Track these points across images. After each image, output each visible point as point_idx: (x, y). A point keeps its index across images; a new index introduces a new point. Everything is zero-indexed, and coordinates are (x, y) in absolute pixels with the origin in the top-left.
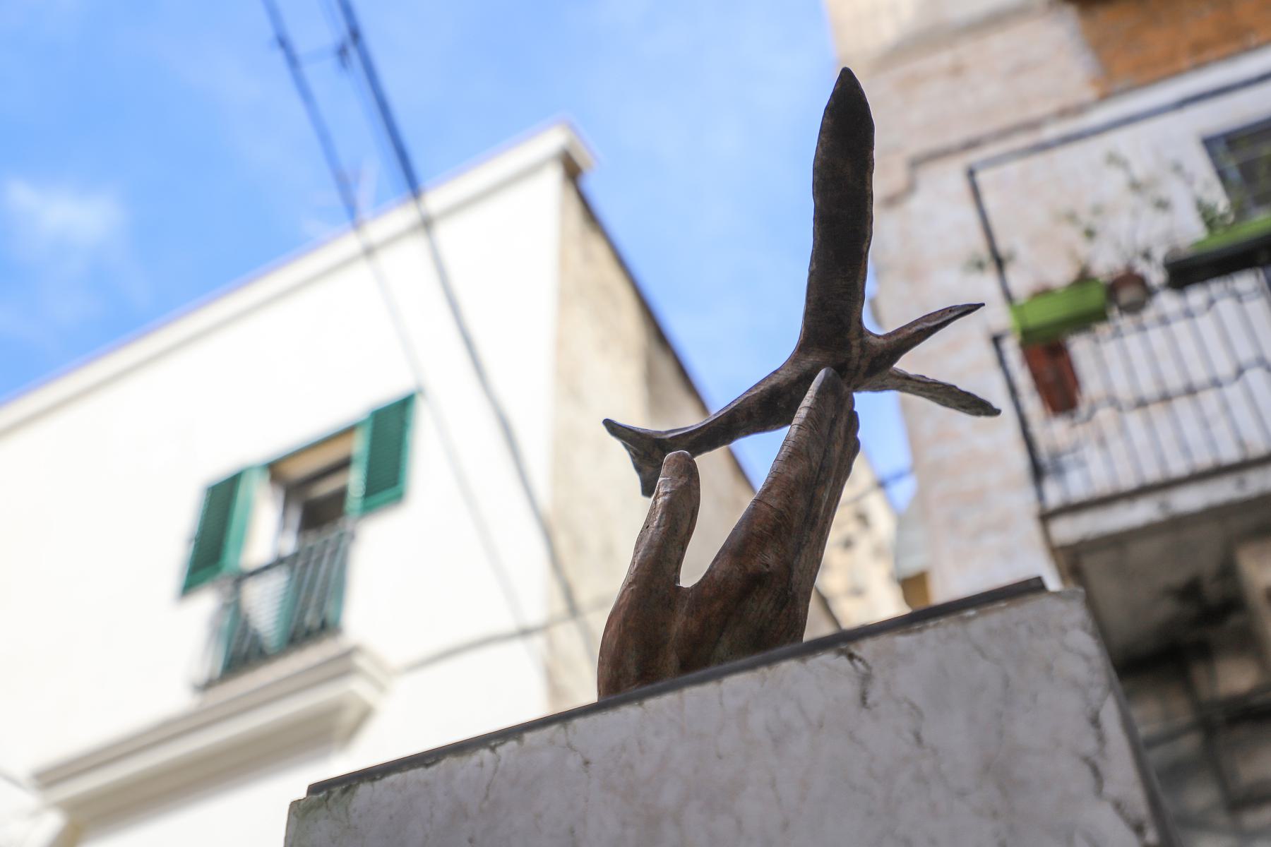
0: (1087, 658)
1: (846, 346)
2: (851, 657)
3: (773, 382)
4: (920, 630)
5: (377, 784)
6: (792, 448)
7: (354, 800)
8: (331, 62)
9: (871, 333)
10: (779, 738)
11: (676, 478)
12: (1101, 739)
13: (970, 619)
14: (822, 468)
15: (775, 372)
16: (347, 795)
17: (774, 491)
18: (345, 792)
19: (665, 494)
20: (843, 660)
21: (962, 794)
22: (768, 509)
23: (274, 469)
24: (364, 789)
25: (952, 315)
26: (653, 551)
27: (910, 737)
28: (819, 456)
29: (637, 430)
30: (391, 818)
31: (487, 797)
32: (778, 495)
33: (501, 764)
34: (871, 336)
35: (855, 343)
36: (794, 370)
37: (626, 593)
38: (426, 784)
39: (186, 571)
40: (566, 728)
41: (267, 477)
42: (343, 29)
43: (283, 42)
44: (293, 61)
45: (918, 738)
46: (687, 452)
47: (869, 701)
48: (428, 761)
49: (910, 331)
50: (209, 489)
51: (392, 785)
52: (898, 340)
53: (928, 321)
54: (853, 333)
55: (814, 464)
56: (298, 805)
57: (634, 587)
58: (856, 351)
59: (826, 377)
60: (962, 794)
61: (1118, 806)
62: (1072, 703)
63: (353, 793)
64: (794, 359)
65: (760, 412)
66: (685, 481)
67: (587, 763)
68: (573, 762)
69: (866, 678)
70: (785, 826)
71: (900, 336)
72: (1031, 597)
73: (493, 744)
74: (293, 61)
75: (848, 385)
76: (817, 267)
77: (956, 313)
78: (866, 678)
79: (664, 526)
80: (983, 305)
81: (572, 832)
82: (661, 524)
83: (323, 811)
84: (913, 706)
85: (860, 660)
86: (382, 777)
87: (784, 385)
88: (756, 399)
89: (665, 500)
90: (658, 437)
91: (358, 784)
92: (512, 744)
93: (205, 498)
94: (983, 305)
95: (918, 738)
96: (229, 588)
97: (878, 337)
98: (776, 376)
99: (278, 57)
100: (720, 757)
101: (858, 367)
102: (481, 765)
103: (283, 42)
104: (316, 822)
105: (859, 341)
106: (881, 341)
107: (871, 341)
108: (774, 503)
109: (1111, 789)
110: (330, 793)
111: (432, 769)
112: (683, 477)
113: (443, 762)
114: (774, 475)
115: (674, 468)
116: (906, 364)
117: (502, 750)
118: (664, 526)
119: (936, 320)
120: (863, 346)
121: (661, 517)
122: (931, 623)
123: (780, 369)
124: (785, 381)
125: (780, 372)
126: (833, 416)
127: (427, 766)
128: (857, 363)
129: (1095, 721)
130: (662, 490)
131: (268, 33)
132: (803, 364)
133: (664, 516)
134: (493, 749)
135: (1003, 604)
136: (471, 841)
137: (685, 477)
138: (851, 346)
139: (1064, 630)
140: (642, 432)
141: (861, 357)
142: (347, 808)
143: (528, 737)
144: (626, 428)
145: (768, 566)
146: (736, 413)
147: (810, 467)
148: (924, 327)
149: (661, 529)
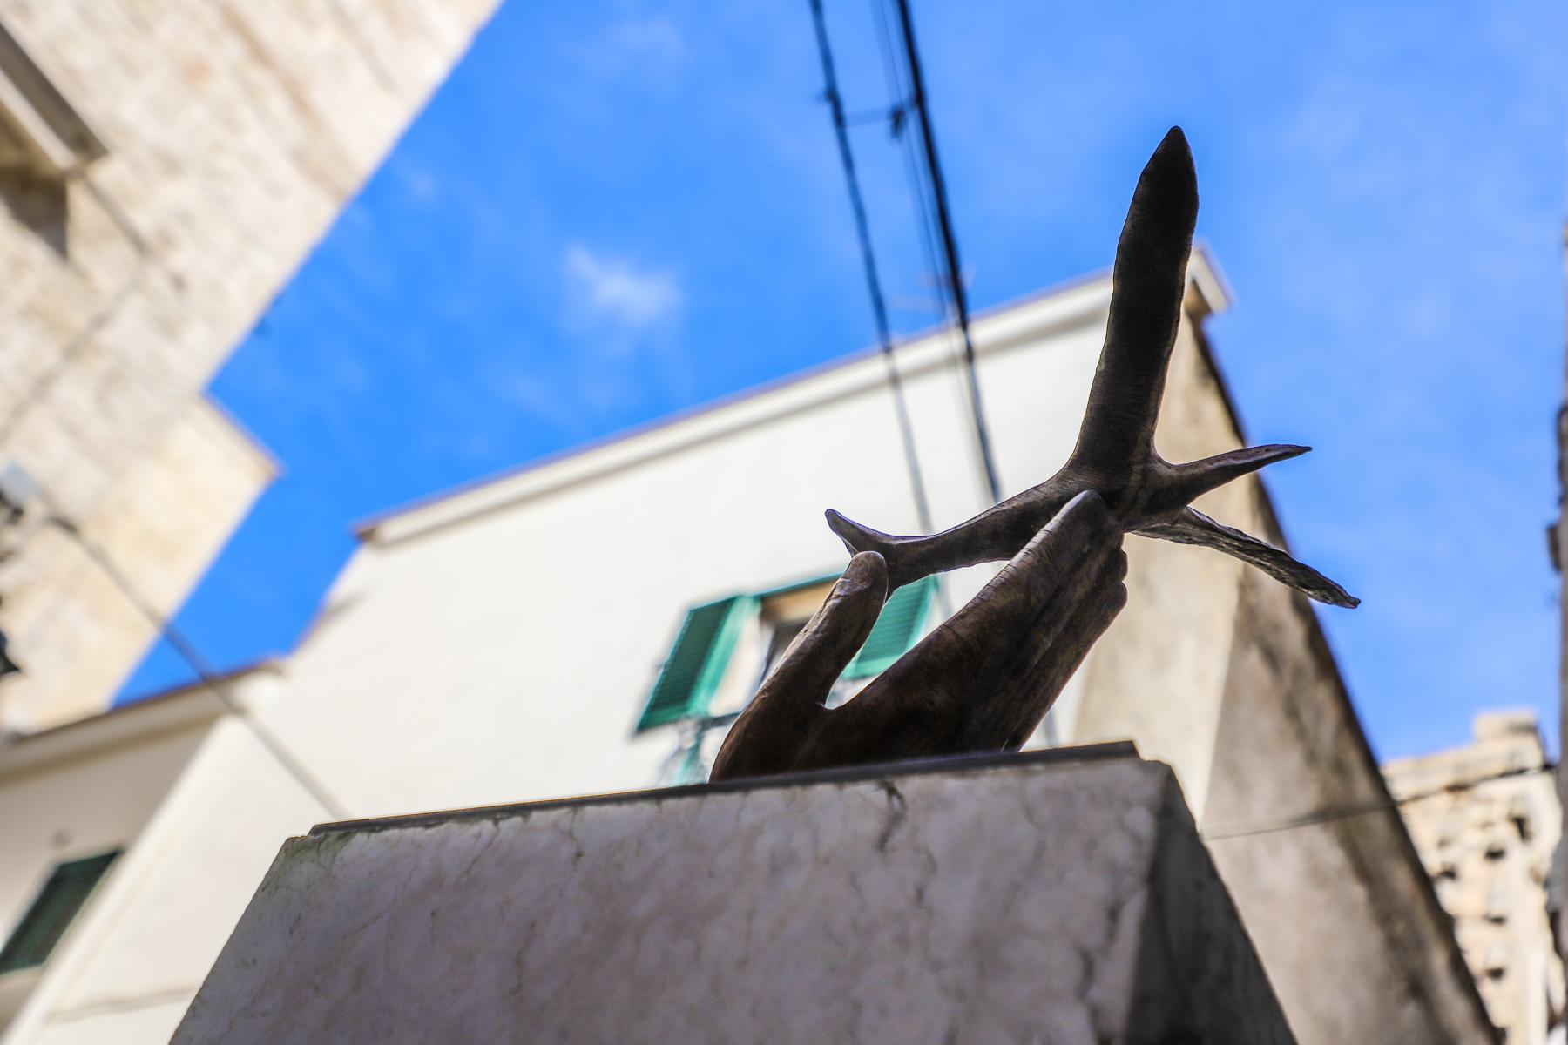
0: (1136, 839)
1: (1125, 469)
2: (892, 791)
3: (1030, 499)
4: (976, 776)
5: (373, 835)
6: (1011, 575)
7: (344, 849)
8: (884, 125)
9: (1160, 460)
10: (780, 865)
11: (856, 581)
12: (1111, 935)
13: (1038, 773)
14: (1048, 607)
15: (1036, 488)
16: (341, 842)
17: (969, 620)
18: (340, 837)
19: (838, 596)
20: (882, 795)
21: (937, 966)
22: (953, 638)
23: (768, 604)
24: (360, 838)
25: (1268, 455)
26: (801, 658)
27: (912, 892)
28: (1046, 592)
29: (861, 528)
30: (371, 873)
31: (468, 872)
32: (972, 624)
33: (497, 839)
34: (1159, 464)
35: (1137, 468)
36: (1057, 489)
37: (756, 701)
38: (419, 846)
39: (647, 704)
40: (575, 813)
41: (757, 610)
42: (905, 90)
43: (833, 97)
44: (839, 120)
45: (920, 893)
46: (879, 554)
47: (888, 845)
48: (431, 822)
49: (1210, 466)
50: (691, 612)
51: (387, 840)
52: (1193, 475)
53: (1235, 458)
54: (1137, 456)
55: (1033, 600)
56: (294, 842)
57: (766, 695)
58: (1135, 478)
59: (1085, 498)
60: (937, 966)
61: (1095, 1013)
62: (1096, 888)
63: (347, 841)
64: (1061, 477)
65: (1008, 532)
66: (865, 587)
67: (579, 855)
68: (567, 850)
69: (895, 819)
70: (743, 963)
71: (1196, 471)
72: (769, 654)
73: (498, 816)
74: (839, 120)
75: (1119, 518)
76: (1106, 367)
77: (1273, 454)
78: (895, 819)
79: (822, 632)
80: (1309, 449)
81: (533, 925)
82: (820, 631)
83: (312, 854)
84: (931, 860)
85: (900, 797)
86: (381, 830)
87: (1041, 504)
88: (1003, 515)
89: (834, 604)
90: (885, 541)
91: (356, 832)
92: (517, 820)
93: (685, 620)
94: (1309, 449)
95: (920, 893)
96: (690, 735)
97: (1169, 466)
98: (1036, 492)
99: (826, 110)
100: (711, 875)
101: (1135, 499)
102: (478, 836)
103: (833, 97)
104: (301, 863)
105: (1141, 467)
106: (1171, 472)
107: (1158, 470)
108: (963, 632)
109: (1097, 993)
110: (326, 836)
111: (430, 831)
112: (865, 583)
113: (444, 826)
114: (977, 601)
115: (859, 569)
116: (1204, 505)
117: (503, 825)
118: (822, 632)
119: (1246, 458)
120: (1146, 474)
121: (822, 623)
122: (990, 771)
123: (1043, 485)
124: (1042, 501)
125: (1041, 489)
126: (1085, 550)
127: (428, 826)
128: (1134, 492)
129: (1113, 914)
130: (837, 592)
131: (820, 84)
132: (1070, 483)
133: (827, 620)
134: (496, 822)
135: (1077, 764)
136: (433, 914)
137: (869, 582)
138: (1132, 471)
139: (1127, 804)
140: (867, 531)
141: (1141, 487)
142: (335, 856)
143: (536, 816)
144: (848, 523)
145: (932, 703)
146: (979, 529)
147: (1027, 603)
148: (1228, 464)
149: (818, 636)
